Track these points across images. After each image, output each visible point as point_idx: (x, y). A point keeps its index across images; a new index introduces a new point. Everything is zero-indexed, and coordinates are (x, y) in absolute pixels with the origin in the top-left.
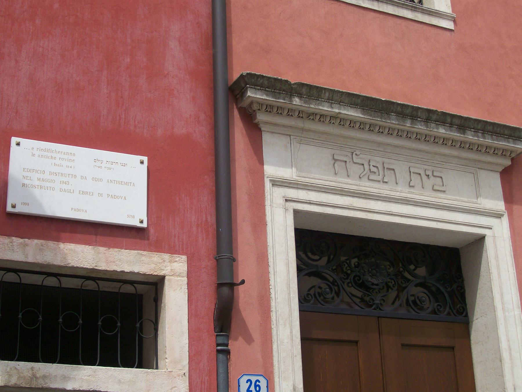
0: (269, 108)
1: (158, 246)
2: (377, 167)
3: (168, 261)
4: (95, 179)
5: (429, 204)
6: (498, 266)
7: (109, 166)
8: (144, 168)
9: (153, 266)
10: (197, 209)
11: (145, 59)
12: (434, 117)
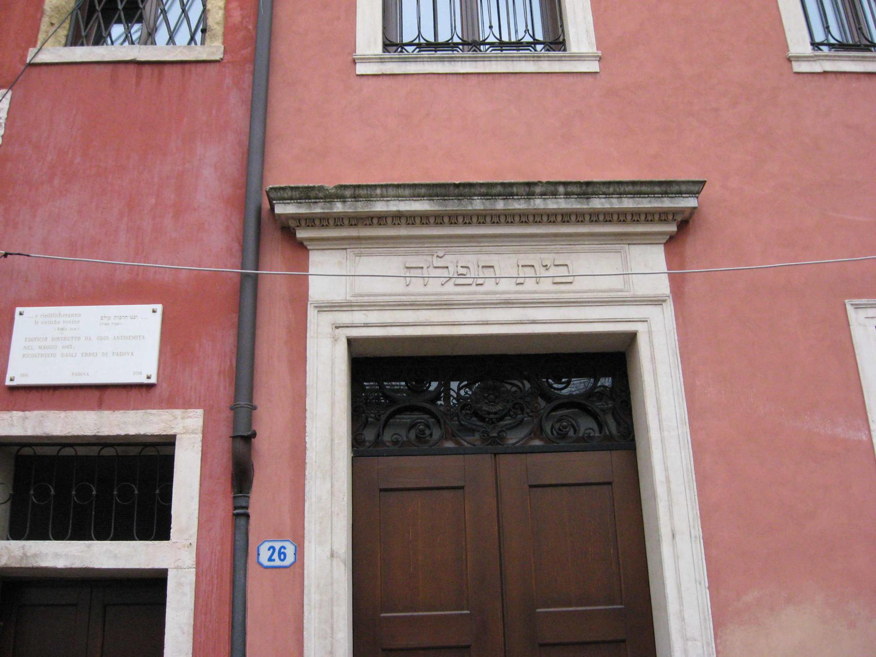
0: (310, 221)
1: (170, 403)
2: (468, 267)
3: (179, 417)
4: (100, 338)
5: (543, 303)
6: (655, 372)
7: (117, 321)
8: (158, 318)
9: (162, 425)
10: (214, 355)
11: (173, 196)
12: (538, 190)
